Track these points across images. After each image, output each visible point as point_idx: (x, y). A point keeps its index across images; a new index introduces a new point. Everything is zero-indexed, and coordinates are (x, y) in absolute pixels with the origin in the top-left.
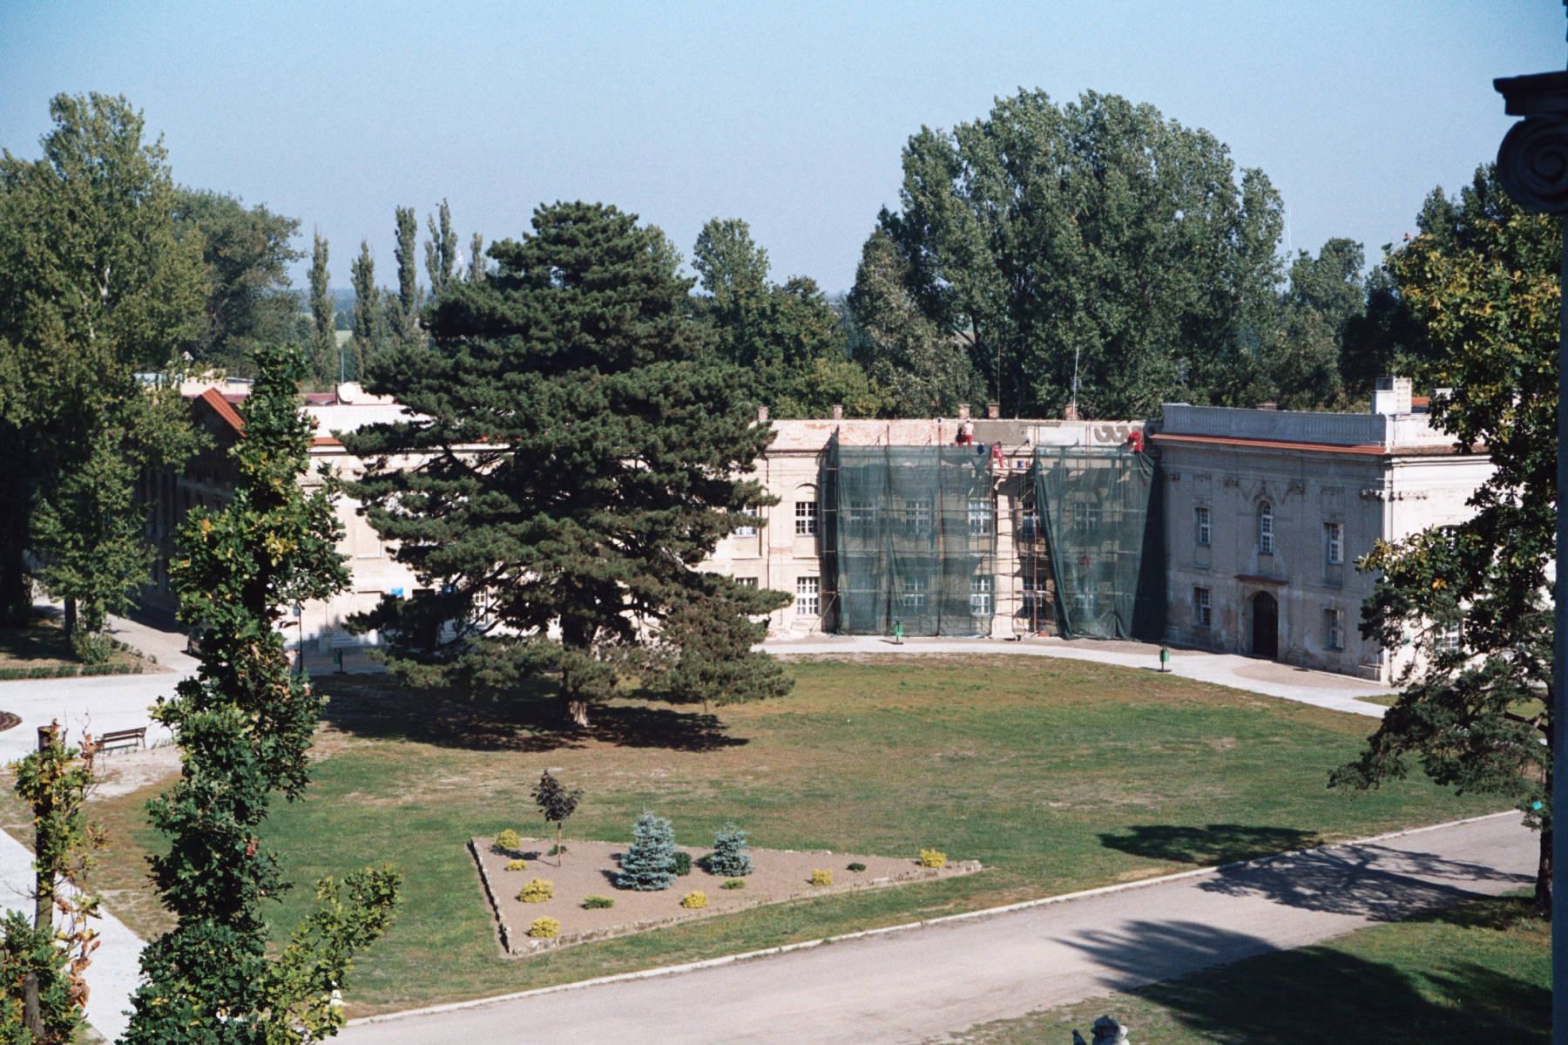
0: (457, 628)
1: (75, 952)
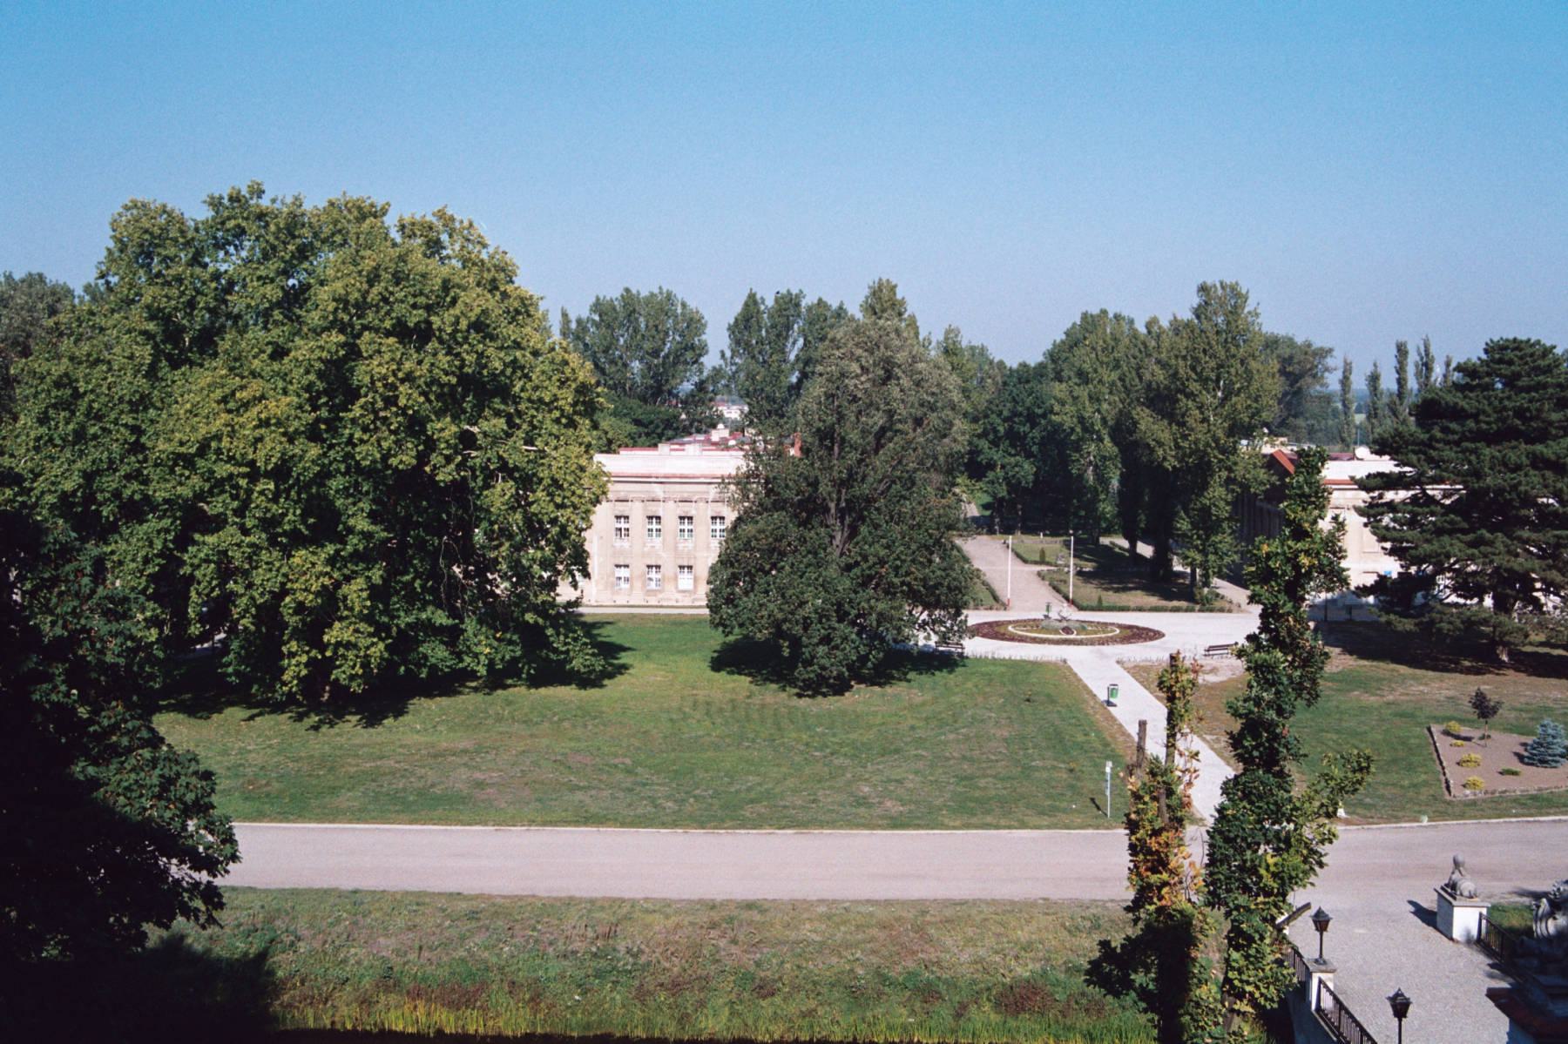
0: (1425, 597)
1: (1187, 778)
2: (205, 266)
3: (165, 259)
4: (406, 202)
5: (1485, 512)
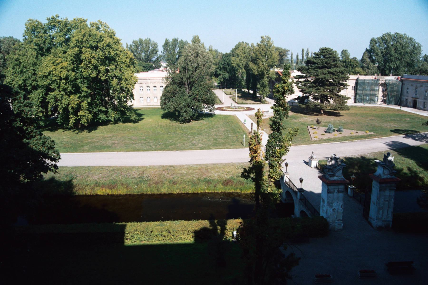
2: (47, 33)
3: (38, 32)
4: (91, 19)
5: (319, 83)
